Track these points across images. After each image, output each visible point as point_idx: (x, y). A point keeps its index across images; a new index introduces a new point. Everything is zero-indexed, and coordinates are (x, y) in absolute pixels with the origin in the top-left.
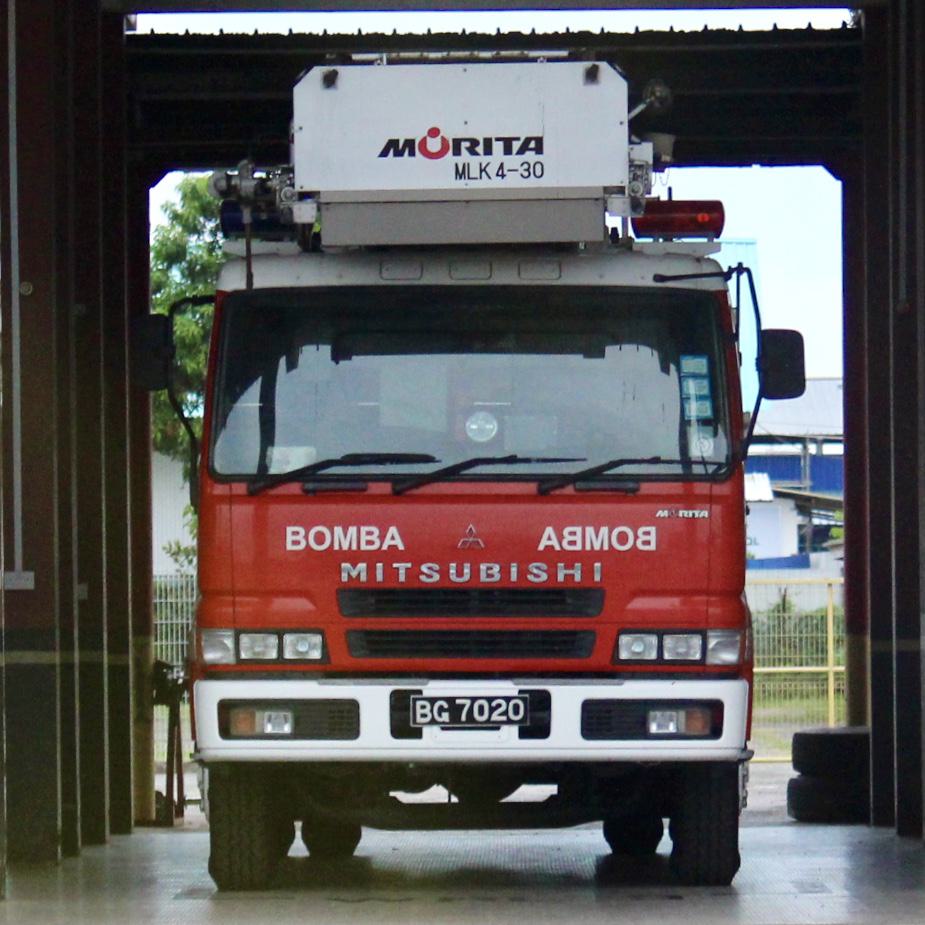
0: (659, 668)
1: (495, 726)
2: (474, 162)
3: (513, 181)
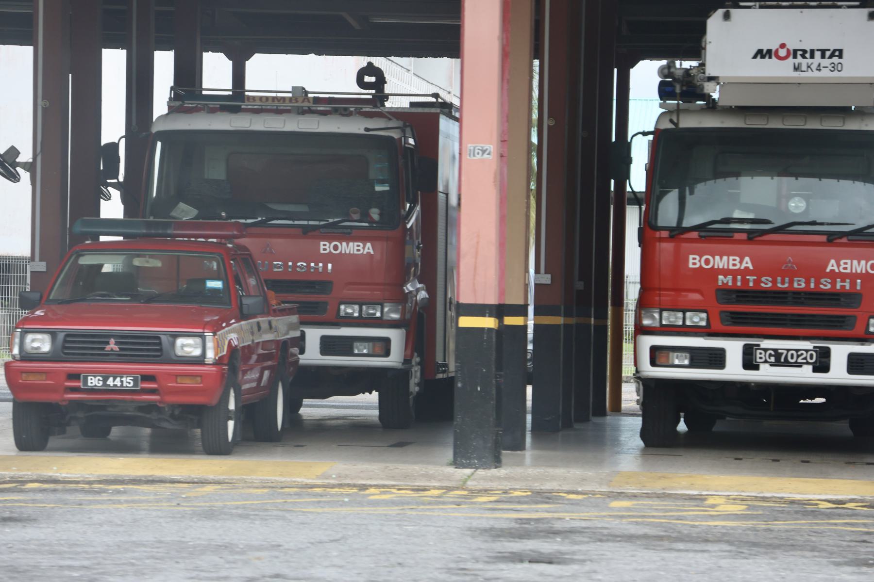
0: (682, 329)
1: (798, 365)
2: (804, 62)
3: (825, 73)
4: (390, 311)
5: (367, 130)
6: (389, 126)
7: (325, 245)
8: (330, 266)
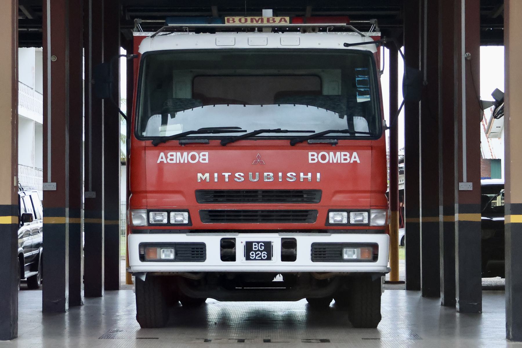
0: (348, 227)
4: (376, 218)
5: (346, 45)
6: (366, 41)
7: (313, 155)
8: (318, 175)
